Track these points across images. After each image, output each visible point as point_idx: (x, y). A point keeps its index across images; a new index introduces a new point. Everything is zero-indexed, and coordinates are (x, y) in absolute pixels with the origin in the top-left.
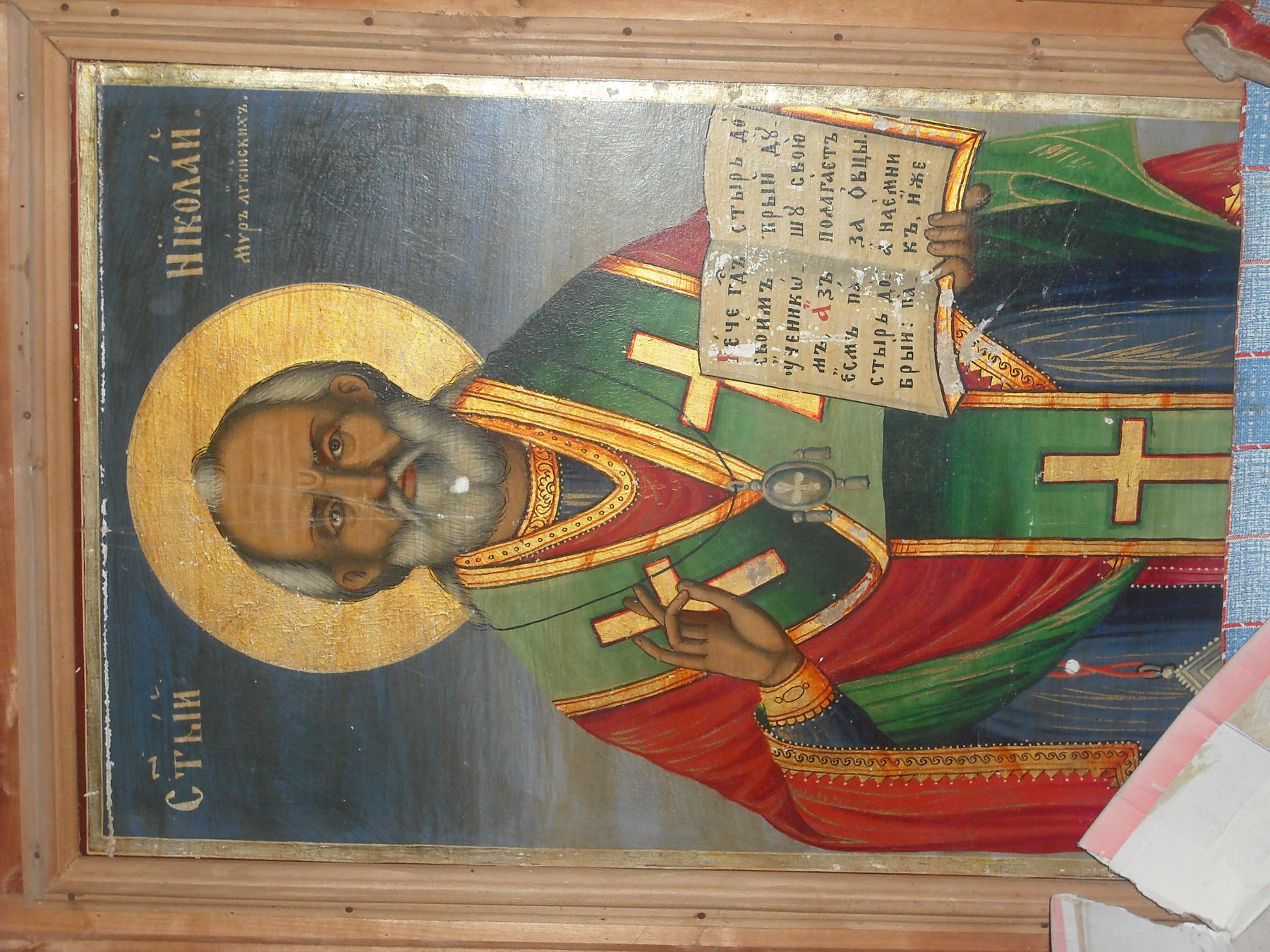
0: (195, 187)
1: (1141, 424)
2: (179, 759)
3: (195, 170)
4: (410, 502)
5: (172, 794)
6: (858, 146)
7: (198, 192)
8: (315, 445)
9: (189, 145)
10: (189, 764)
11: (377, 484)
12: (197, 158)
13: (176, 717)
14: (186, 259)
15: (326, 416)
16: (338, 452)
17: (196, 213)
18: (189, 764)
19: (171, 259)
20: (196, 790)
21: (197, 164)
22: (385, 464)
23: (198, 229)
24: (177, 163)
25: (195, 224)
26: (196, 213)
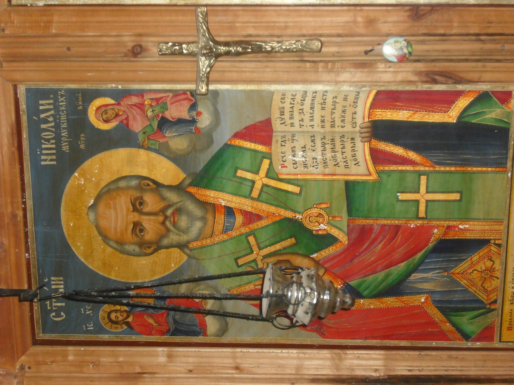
0: (52, 127)
1: (299, 188)
2: (55, 302)
3: (51, 119)
4: (174, 224)
5: (54, 314)
6: (357, 94)
7: (53, 130)
8: (134, 205)
9: (47, 107)
10: (59, 304)
11: (161, 218)
12: (52, 112)
13: (43, 163)
14: (49, 158)
15: (137, 194)
16: (142, 207)
17: (52, 139)
18: (59, 304)
19: (43, 157)
20: (62, 314)
21: (52, 115)
22: (163, 211)
23: (54, 146)
24: (42, 116)
25: (52, 144)
26: (52, 139)
